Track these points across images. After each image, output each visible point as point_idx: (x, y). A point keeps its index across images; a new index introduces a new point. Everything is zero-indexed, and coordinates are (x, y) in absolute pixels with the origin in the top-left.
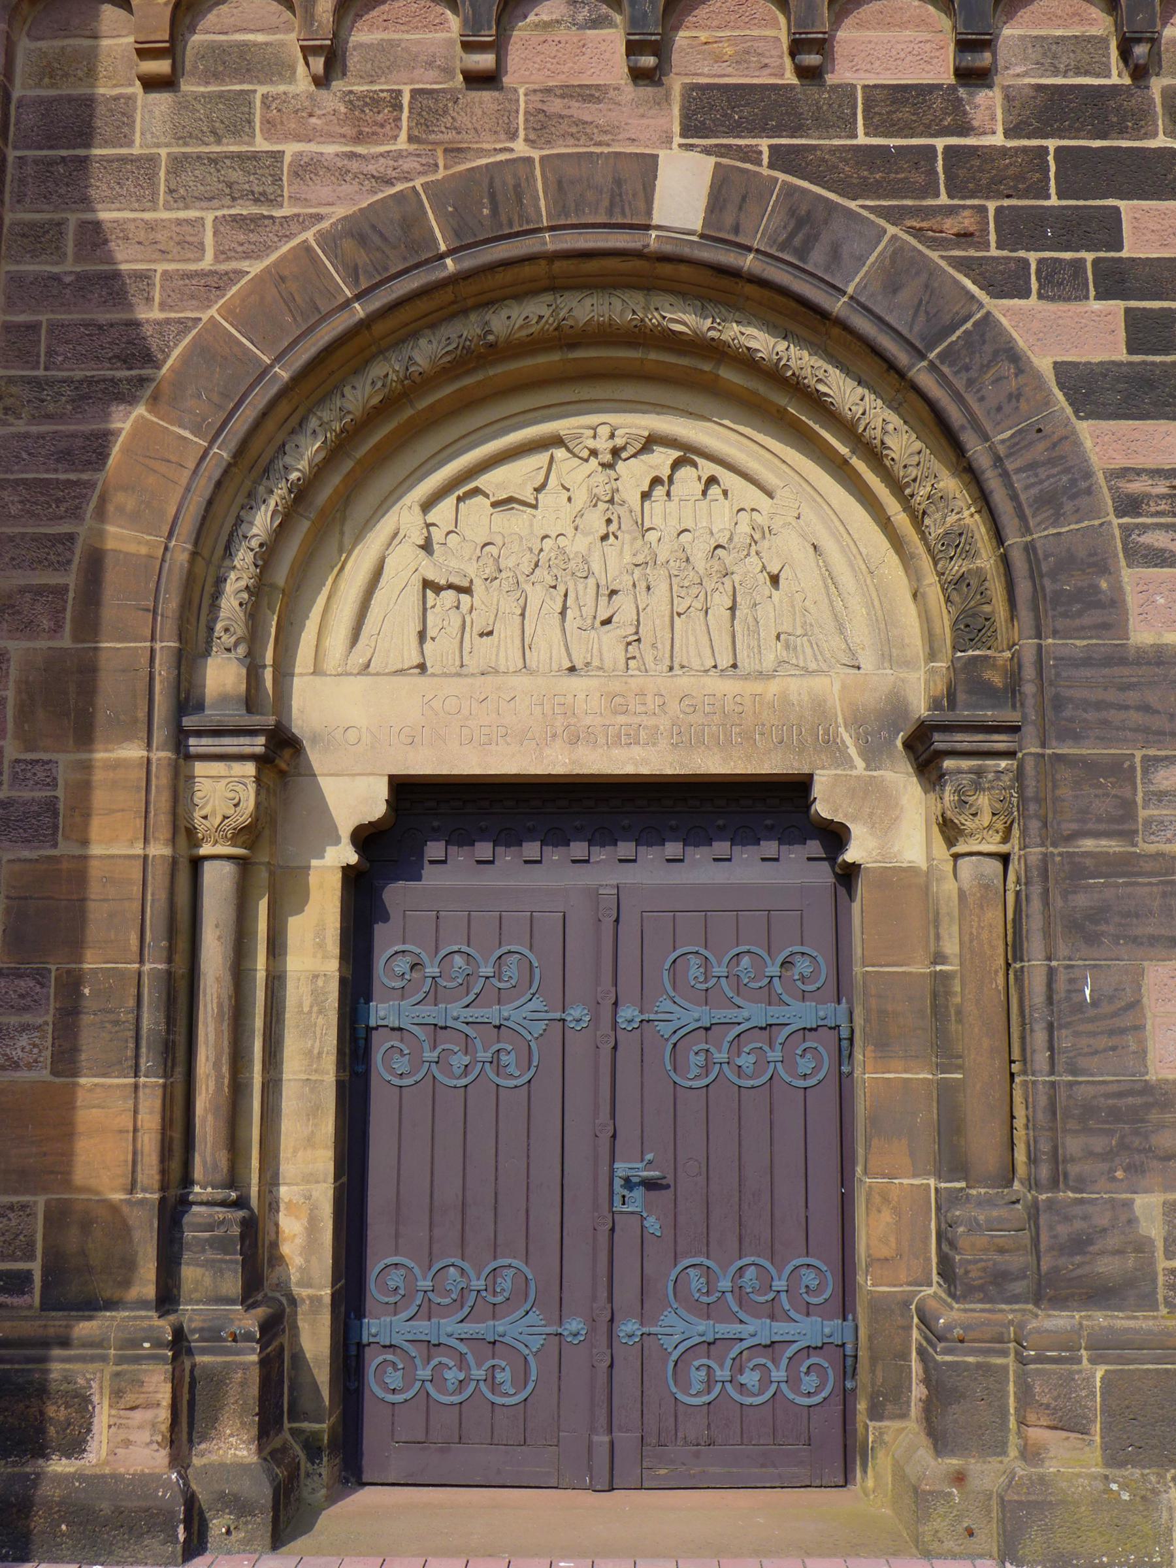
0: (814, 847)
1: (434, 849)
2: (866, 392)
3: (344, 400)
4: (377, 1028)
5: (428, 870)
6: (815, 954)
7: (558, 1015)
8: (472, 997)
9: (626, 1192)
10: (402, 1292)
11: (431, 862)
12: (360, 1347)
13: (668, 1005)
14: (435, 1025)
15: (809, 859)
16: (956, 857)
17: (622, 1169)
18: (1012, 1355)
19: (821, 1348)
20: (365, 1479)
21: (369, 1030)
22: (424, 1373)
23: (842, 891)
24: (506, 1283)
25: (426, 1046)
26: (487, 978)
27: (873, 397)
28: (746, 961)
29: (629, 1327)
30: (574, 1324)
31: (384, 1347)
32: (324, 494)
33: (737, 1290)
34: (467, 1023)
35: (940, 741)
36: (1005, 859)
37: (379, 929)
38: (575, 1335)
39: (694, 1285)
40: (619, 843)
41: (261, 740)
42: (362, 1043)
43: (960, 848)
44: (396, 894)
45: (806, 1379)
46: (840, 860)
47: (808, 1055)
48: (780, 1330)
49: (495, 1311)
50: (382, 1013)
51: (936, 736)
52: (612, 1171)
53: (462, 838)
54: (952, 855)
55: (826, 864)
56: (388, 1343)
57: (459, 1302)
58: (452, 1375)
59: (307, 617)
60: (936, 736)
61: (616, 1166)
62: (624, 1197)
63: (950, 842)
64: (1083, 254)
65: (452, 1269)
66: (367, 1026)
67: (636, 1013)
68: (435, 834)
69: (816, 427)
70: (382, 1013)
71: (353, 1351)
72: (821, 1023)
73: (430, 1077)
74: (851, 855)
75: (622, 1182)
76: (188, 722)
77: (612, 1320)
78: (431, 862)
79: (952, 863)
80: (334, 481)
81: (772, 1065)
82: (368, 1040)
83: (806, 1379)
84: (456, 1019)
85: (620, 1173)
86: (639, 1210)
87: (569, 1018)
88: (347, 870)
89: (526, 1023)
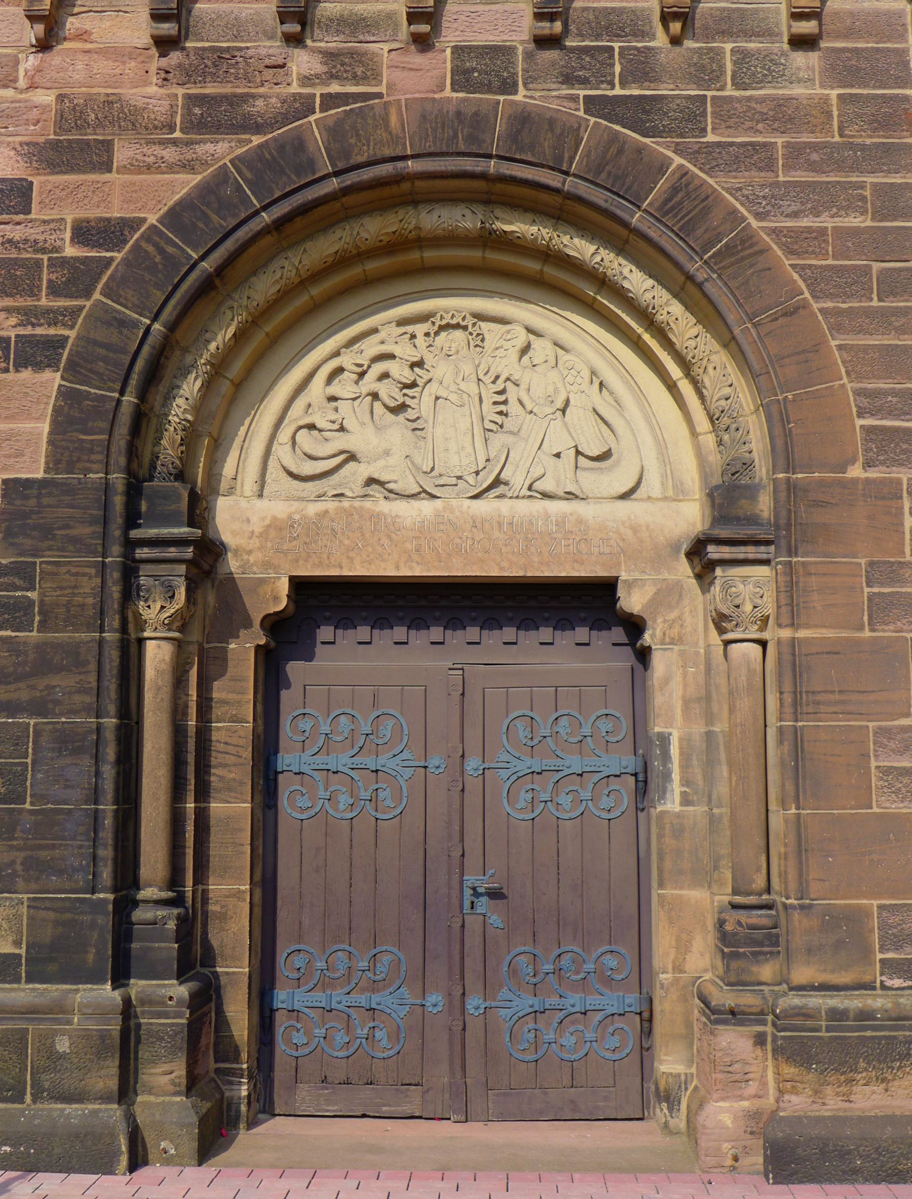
0: (618, 634)
1: (325, 633)
2: (656, 284)
3: (251, 290)
4: (282, 772)
5: (319, 649)
6: (618, 715)
7: (418, 1002)
8: (356, 749)
9: (473, 898)
10: (307, 734)
11: (323, 643)
12: (273, 1011)
13: (504, 757)
14: (328, 770)
15: (614, 644)
16: (727, 643)
17: (471, 879)
18: (770, 1024)
19: (623, 1015)
20: (277, 1112)
21: (277, 773)
22: (319, 1032)
23: (639, 667)
24: (382, 968)
25: (321, 788)
26: (367, 735)
27: (660, 287)
28: (564, 721)
29: (474, 1003)
30: (434, 996)
31: (296, 774)
32: (236, 369)
33: (554, 734)
34: (349, 1007)
35: (714, 552)
36: (763, 644)
37: (284, 694)
38: (435, 1006)
39: (521, 734)
40: (467, 628)
41: (191, 549)
42: (267, 1021)
43: (730, 636)
44: (294, 669)
45: (605, 798)
46: (638, 645)
47: (612, 796)
48: (593, 1000)
49: (374, 986)
50: (287, 761)
51: (711, 548)
52: (462, 882)
53: (345, 623)
54: (722, 641)
55: (629, 648)
56: (297, 771)
57: (350, 740)
58: (341, 1038)
59: (225, 462)
60: (711, 548)
61: (465, 878)
62: (472, 903)
63: (721, 631)
64: (872, 902)
65: (342, 718)
66: (276, 771)
67: (481, 1001)
68: (327, 621)
69: (619, 312)
70: (287, 761)
71: (267, 1014)
72: (623, 771)
73: (323, 812)
74: (647, 638)
75: (472, 892)
76: (134, 534)
77: (464, 994)
78: (323, 643)
79: (722, 647)
80: (248, 351)
81: (588, 1043)
82: (276, 780)
83: (605, 798)
84: (339, 1003)
85: (469, 884)
86: (484, 911)
87: (428, 1004)
88: (258, 648)
89: (398, 768)
